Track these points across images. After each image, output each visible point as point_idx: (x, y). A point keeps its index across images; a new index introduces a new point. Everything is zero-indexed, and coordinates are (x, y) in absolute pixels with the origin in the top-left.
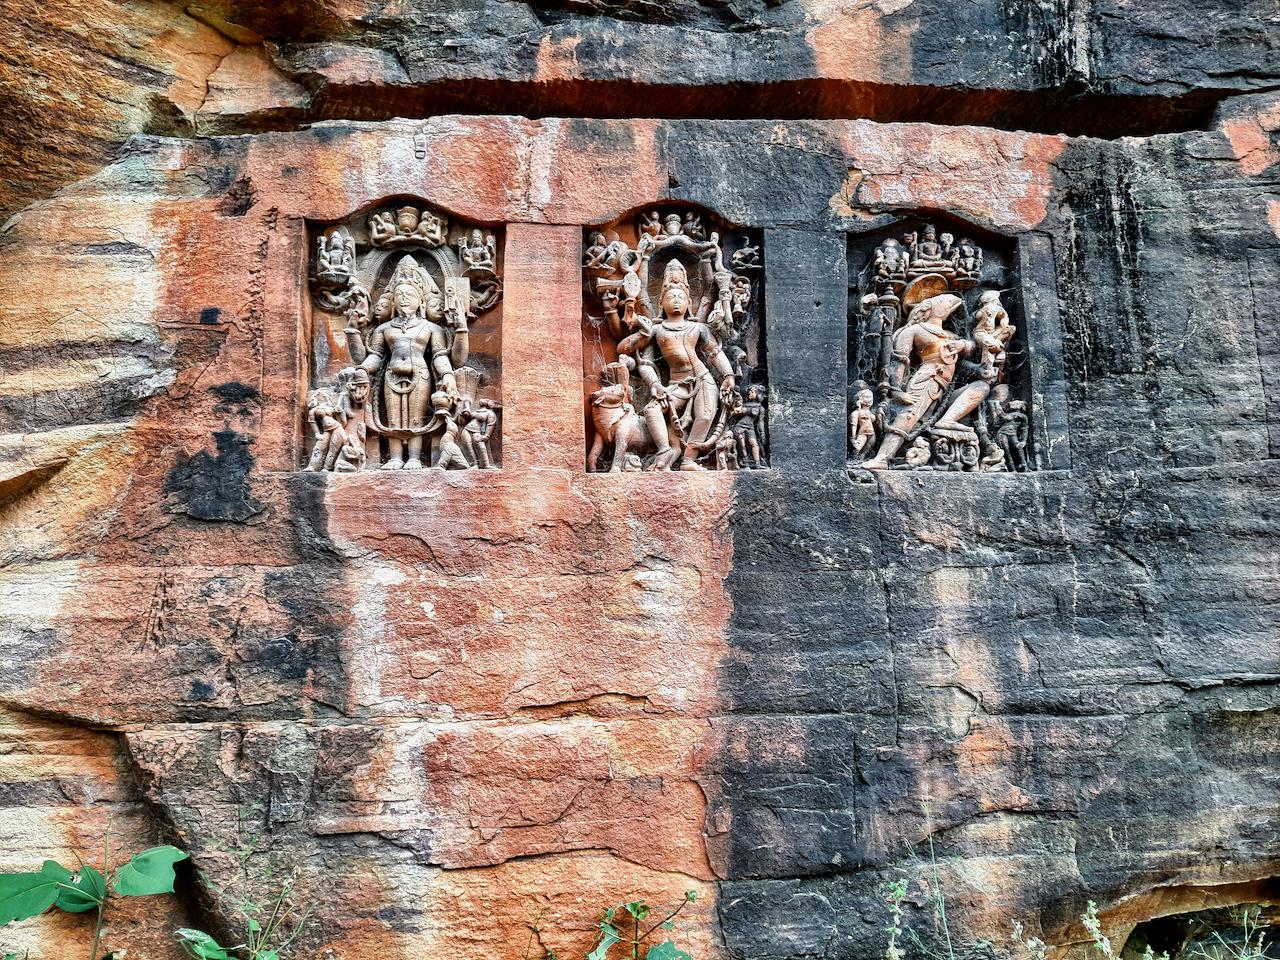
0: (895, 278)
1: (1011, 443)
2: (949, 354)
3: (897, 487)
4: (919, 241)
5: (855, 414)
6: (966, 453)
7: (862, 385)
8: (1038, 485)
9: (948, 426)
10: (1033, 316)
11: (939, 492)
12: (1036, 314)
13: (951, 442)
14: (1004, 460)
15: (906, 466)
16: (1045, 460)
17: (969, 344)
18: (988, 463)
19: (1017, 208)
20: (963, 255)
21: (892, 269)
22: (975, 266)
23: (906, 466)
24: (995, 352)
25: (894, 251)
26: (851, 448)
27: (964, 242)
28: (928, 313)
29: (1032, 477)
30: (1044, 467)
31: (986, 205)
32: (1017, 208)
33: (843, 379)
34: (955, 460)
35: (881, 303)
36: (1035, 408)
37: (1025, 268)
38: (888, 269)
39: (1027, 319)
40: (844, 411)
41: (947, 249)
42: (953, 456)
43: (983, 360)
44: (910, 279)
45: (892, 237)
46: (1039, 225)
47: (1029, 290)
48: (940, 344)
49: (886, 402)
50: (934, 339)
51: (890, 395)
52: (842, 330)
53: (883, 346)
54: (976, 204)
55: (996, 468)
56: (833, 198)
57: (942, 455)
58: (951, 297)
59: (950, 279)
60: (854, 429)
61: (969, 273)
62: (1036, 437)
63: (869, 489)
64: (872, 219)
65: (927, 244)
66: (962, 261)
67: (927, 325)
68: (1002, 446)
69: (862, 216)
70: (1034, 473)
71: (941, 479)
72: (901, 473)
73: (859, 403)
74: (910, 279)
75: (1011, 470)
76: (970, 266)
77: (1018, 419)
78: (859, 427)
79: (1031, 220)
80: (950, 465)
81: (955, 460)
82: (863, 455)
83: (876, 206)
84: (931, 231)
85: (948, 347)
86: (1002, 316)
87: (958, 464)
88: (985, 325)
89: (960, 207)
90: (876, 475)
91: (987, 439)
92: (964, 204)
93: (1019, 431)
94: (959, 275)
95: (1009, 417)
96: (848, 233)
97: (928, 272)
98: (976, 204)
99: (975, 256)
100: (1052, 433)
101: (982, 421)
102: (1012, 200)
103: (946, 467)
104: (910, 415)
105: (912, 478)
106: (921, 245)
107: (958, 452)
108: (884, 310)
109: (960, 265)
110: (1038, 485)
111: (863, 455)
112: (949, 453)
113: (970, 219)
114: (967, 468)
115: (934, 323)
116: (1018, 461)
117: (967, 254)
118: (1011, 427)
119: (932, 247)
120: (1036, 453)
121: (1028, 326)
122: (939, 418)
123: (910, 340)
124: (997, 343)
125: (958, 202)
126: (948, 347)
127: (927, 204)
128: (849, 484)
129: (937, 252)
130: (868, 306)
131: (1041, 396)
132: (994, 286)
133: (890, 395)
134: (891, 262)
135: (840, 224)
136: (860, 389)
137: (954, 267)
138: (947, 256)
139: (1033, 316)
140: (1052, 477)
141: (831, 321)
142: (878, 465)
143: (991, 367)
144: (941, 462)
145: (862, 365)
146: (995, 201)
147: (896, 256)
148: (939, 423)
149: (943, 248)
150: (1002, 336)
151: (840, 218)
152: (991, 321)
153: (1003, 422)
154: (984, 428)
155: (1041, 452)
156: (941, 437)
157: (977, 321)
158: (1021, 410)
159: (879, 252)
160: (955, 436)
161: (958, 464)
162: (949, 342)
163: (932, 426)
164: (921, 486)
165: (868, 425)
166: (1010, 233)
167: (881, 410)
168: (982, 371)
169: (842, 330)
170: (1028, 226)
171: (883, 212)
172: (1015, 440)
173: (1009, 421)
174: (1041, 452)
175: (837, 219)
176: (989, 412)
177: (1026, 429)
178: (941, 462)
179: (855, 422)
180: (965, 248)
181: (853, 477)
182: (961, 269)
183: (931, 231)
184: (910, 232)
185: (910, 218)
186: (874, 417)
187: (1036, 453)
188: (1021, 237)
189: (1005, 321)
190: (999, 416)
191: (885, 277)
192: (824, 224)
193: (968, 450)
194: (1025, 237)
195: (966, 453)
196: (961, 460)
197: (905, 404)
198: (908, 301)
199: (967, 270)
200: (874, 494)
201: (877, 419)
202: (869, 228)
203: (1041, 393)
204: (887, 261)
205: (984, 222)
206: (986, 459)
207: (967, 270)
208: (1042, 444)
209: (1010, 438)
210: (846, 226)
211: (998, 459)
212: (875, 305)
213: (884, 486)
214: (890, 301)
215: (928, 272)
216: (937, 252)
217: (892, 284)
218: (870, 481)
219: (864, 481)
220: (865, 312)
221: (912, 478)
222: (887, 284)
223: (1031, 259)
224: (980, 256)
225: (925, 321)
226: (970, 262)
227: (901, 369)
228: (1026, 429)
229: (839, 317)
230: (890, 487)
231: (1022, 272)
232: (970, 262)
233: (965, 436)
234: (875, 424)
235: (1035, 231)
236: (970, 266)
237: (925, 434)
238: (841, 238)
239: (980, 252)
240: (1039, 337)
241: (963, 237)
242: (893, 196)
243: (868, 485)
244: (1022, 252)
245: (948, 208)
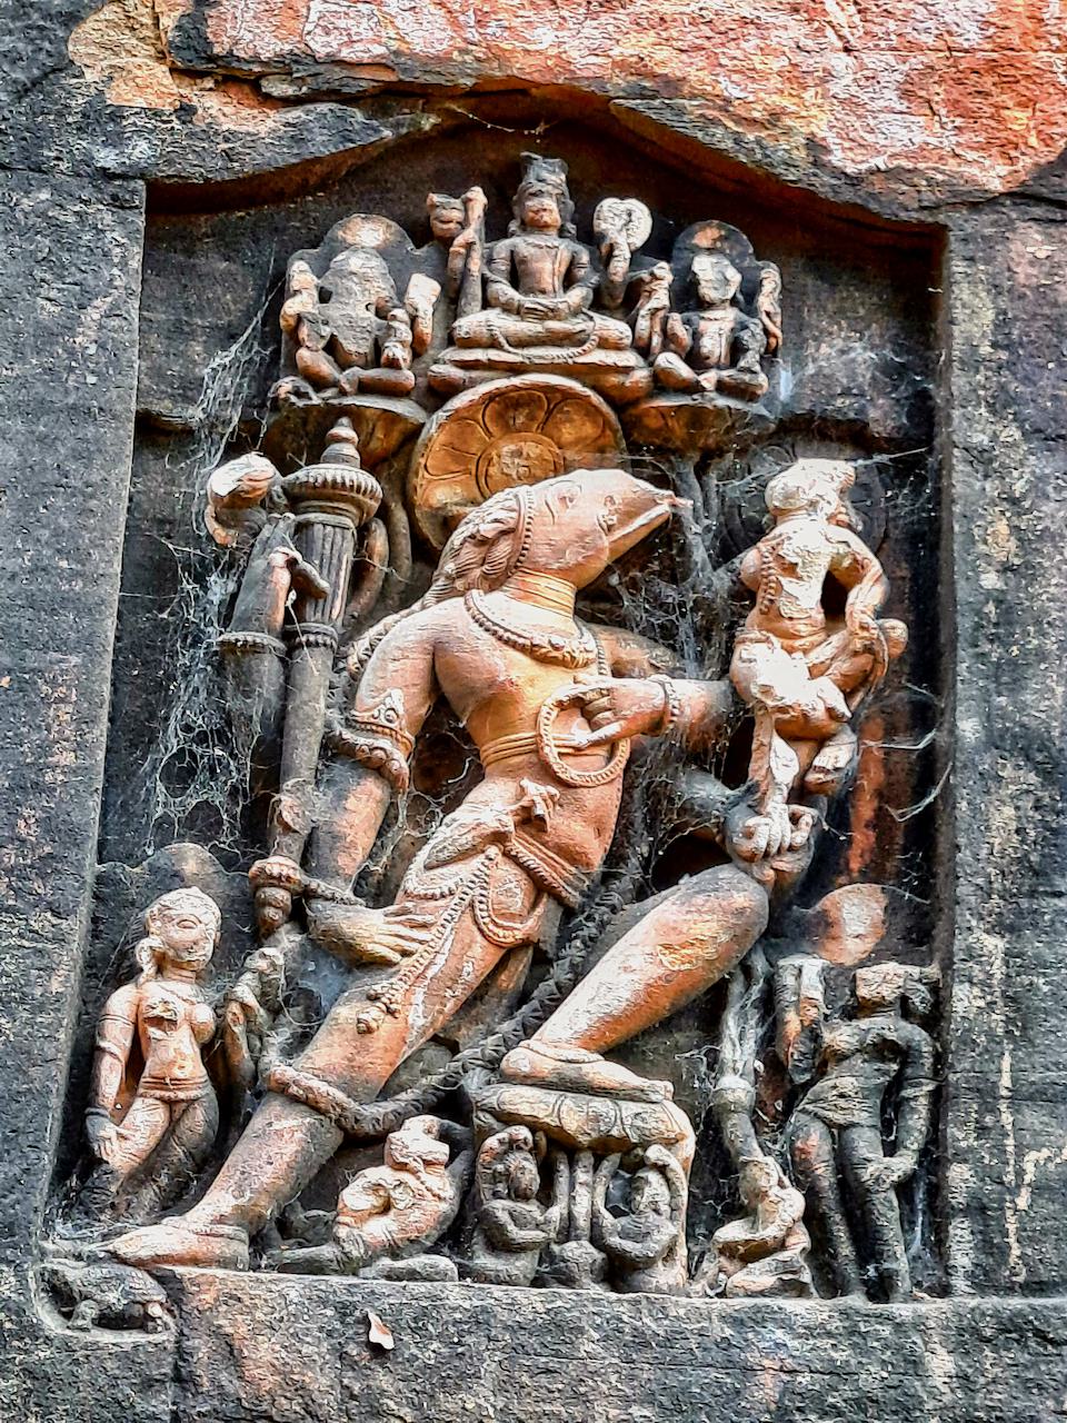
0: (364, 388)
1: (844, 1162)
2: (580, 734)
3: (263, 1353)
4: (496, 227)
5: (121, 1002)
6: (622, 1205)
7: (190, 867)
8: (941, 1363)
9: (546, 1067)
10: (991, 580)
11: (465, 1379)
12: (1006, 569)
13: (555, 1149)
14: (801, 1240)
15: (327, 1251)
16: (990, 1247)
17: (693, 696)
18: (729, 1250)
19: (938, 93)
20: (688, 296)
21: (354, 345)
22: (736, 349)
23: (327, 1251)
24: (806, 733)
25: (376, 266)
26: (78, 1157)
27: (705, 236)
28: (503, 549)
29: (920, 1325)
30: (984, 1281)
31: (795, 78)
32: (938, 93)
33: (73, 836)
34: (568, 1231)
35: (297, 499)
36: (964, 1000)
37: (973, 363)
38: (332, 347)
39: (963, 591)
40: (63, 981)
41: (620, 267)
42: (556, 1212)
43: (756, 770)
44: (437, 394)
45: (369, 209)
46: (1044, 172)
47: (982, 459)
48: (543, 689)
49: (285, 944)
50: (514, 668)
51: (298, 915)
52: (91, 610)
53: (286, 693)
54: (751, 74)
55: (760, 1275)
56: (90, 27)
57: (500, 1208)
58: (618, 484)
59: (623, 403)
60: (110, 1076)
61: (346, 378)
62: (959, 1135)
63: (127, 1358)
64: (266, 124)
65: (523, 244)
66: (676, 323)
67: (498, 605)
68: (797, 1170)
69: (219, 109)
70: (932, 1307)
71: (479, 1319)
72: (295, 1287)
73: (143, 955)
74: (437, 394)
75: (832, 1284)
76: (714, 344)
77: (883, 1049)
78: (135, 1063)
79: (1008, 149)
80: (546, 1255)
81: (568, 1231)
82: (148, 1195)
83: (285, 66)
84: (547, 181)
85: (580, 706)
86: (857, 571)
87: (580, 1252)
88: (773, 616)
89: (673, 85)
90: (176, 1293)
91: (739, 1129)
92: (694, 71)
93: (891, 1105)
94: (662, 383)
95: (841, 1036)
96: (155, 188)
97: (515, 369)
98: (751, 74)
99: (747, 299)
100: (1033, 1118)
101: (739, 1046)
102: (917, 61)
103: (523, 1265)
104: (373, 1013)
105: (344, 1311)
106: (502, 247)
107: (585, 1193)
108: (302, 529)
109: (669, 340)
110: (941, 1363)
111: (148, 1195)
112: (546, 1196)
113: (720, 138)
114: (619, 1271)
115: (527, 595)
116: (868, 1244)
117: (708, 291)
118: (848, 1083)
119: (548, 254)
120: (952, 1212)
121: (965, 623)
122: (528, 1030)
123: (418, 663)
124: (819, 697)
125: (668, 62)
126: (580, 706)
127: (523, 67)
128: (33, 1331)
129: (569, 281)
130: (236, 505)
131: (995, 944)
132: (849, 436)
133: (298, 915)
134: (353, 316)
135: (116, 140)
136: (172, 879)
137: (644, 350)
138: (622, 299)
139: (991, 580)
140: (1014, 1330)
141: (39, 569)
142: (193, 1245)
143: (777, 805)
144: (501, 1245)
145: (181, 774)
146: (840, 62)
147: (382, 288)
148: (520, 1059)
149: (603, 260)
150: (844, 666)
151: (117, 115)
152: (805, 596)
153: (823, 1060)
154: (737, 1086)
155: (978, 1209)
156: (508, 1119)
157: (745, 594)
158: (905, 1008)
159: (301, 273)
160: (573, 1115)
161: (580, 1252)
162: (592, 681)
163: (493, 1065)
164: (377, 1350)
165: (180, 1056)
166: (904, 205)
167: (246, 990)
168: (741, 820)
169: (91, 610)
170: (994, 176)
171: (314, 97)
172: (866, 1143)
173: (841, 1057)
174: (978, 1209)
175: (104, 119)
176: (769, 1005)
177: (919, 1096)
178: (501, 1245)
179: (116, 1039)
180: (704, 266)
181: (63, 1297)
182: (670, 361)
183: (547, 181)
184: (456, 189)
185: (454, 133)
186: (205, 1015)
187: (952, 1212)
188: (960, 223)
189: (866, 597)
190: (812, 1033)
191: (319, 383)
192: (39, 137)
193: (633, 1186)
194: (983, 224)
195: (622, 1205)
196: (597, 1239)
197: (359, 962)
198: (439, 493)
199: (695, 359)
200: (148, 1385)
201: (221, 1031)
202: (248, 165)
203: (1000, 927)
204: (333, 310)
205: (786, 154)
206: (733, 1231)
207: (695, 359)
208: (984, 1174)
209: (839, 1134)
210: (140, 150)
211: (770, 1232)
212: (267, 503)
213: (201, 1347)
214: (330, 494)
215: (515, 369)
216: (569, 281)
217: (356, 416)
218: (142, 1322)
219: (109, 1320)
220: (220, 534)
221: (344, 1311)
222: (333, 414)
223: (1002, 323)
224: (767, 301)
225: (494, 582)
226: (715, 331)
227: (363, 802)
228: (919, 1096)
229: (80, 555)
230: (231, 1354)
231: (959, 381)
232: (715, 331)
233: (623, 1118)
234: (215, 1051)
235: (1022, 196)
236: (714, 344)
237: (450, 1104)
238: (117, 203)
239: (771, 278)
240: (1009, 675)
241: (702, 215)
242: (363, 28)
243: (128, 1338)
244: (962, 292)
245: (619, 82)
